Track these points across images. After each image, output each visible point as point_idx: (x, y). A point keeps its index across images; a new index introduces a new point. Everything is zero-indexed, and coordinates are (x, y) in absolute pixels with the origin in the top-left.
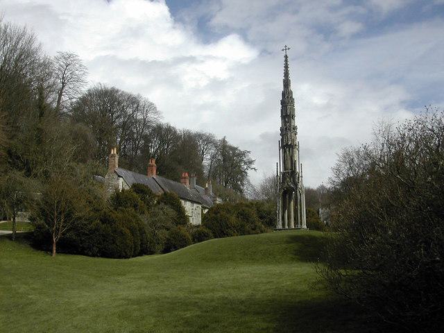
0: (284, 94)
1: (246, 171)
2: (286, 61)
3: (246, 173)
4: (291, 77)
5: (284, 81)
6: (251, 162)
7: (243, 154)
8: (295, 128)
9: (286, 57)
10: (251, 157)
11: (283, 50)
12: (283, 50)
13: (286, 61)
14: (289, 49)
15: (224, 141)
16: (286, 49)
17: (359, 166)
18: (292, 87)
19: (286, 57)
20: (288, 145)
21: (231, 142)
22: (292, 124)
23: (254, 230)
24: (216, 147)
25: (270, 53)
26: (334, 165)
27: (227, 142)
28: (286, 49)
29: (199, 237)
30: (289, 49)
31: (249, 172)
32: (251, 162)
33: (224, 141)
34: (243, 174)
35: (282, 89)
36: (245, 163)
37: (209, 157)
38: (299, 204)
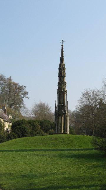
0: (60, 65)
2: (62, 48)
3: (23, 100)
4: (64, 57)
6: (26, 93)
8: (65, 83)
9: (62, 46)
10: (27, 89)
13: (62, 48)
14: (64, 42)
15: (10, 79)
16: (62, 42)
17: (93, 100)
18: (65, 62)
19: (62, 46)
20: (61, 92)
21: (15, 80)
23: (39, 134)
24: (5, 83)
26: (80, 99)
27: (12, 80)
28: (62, 42)
29: (9, 138)
30: (64, 42)
31: (25, 100)
32: (26, 93)
33: (10, 79)
34: (20, 101)
36: (23, 94)
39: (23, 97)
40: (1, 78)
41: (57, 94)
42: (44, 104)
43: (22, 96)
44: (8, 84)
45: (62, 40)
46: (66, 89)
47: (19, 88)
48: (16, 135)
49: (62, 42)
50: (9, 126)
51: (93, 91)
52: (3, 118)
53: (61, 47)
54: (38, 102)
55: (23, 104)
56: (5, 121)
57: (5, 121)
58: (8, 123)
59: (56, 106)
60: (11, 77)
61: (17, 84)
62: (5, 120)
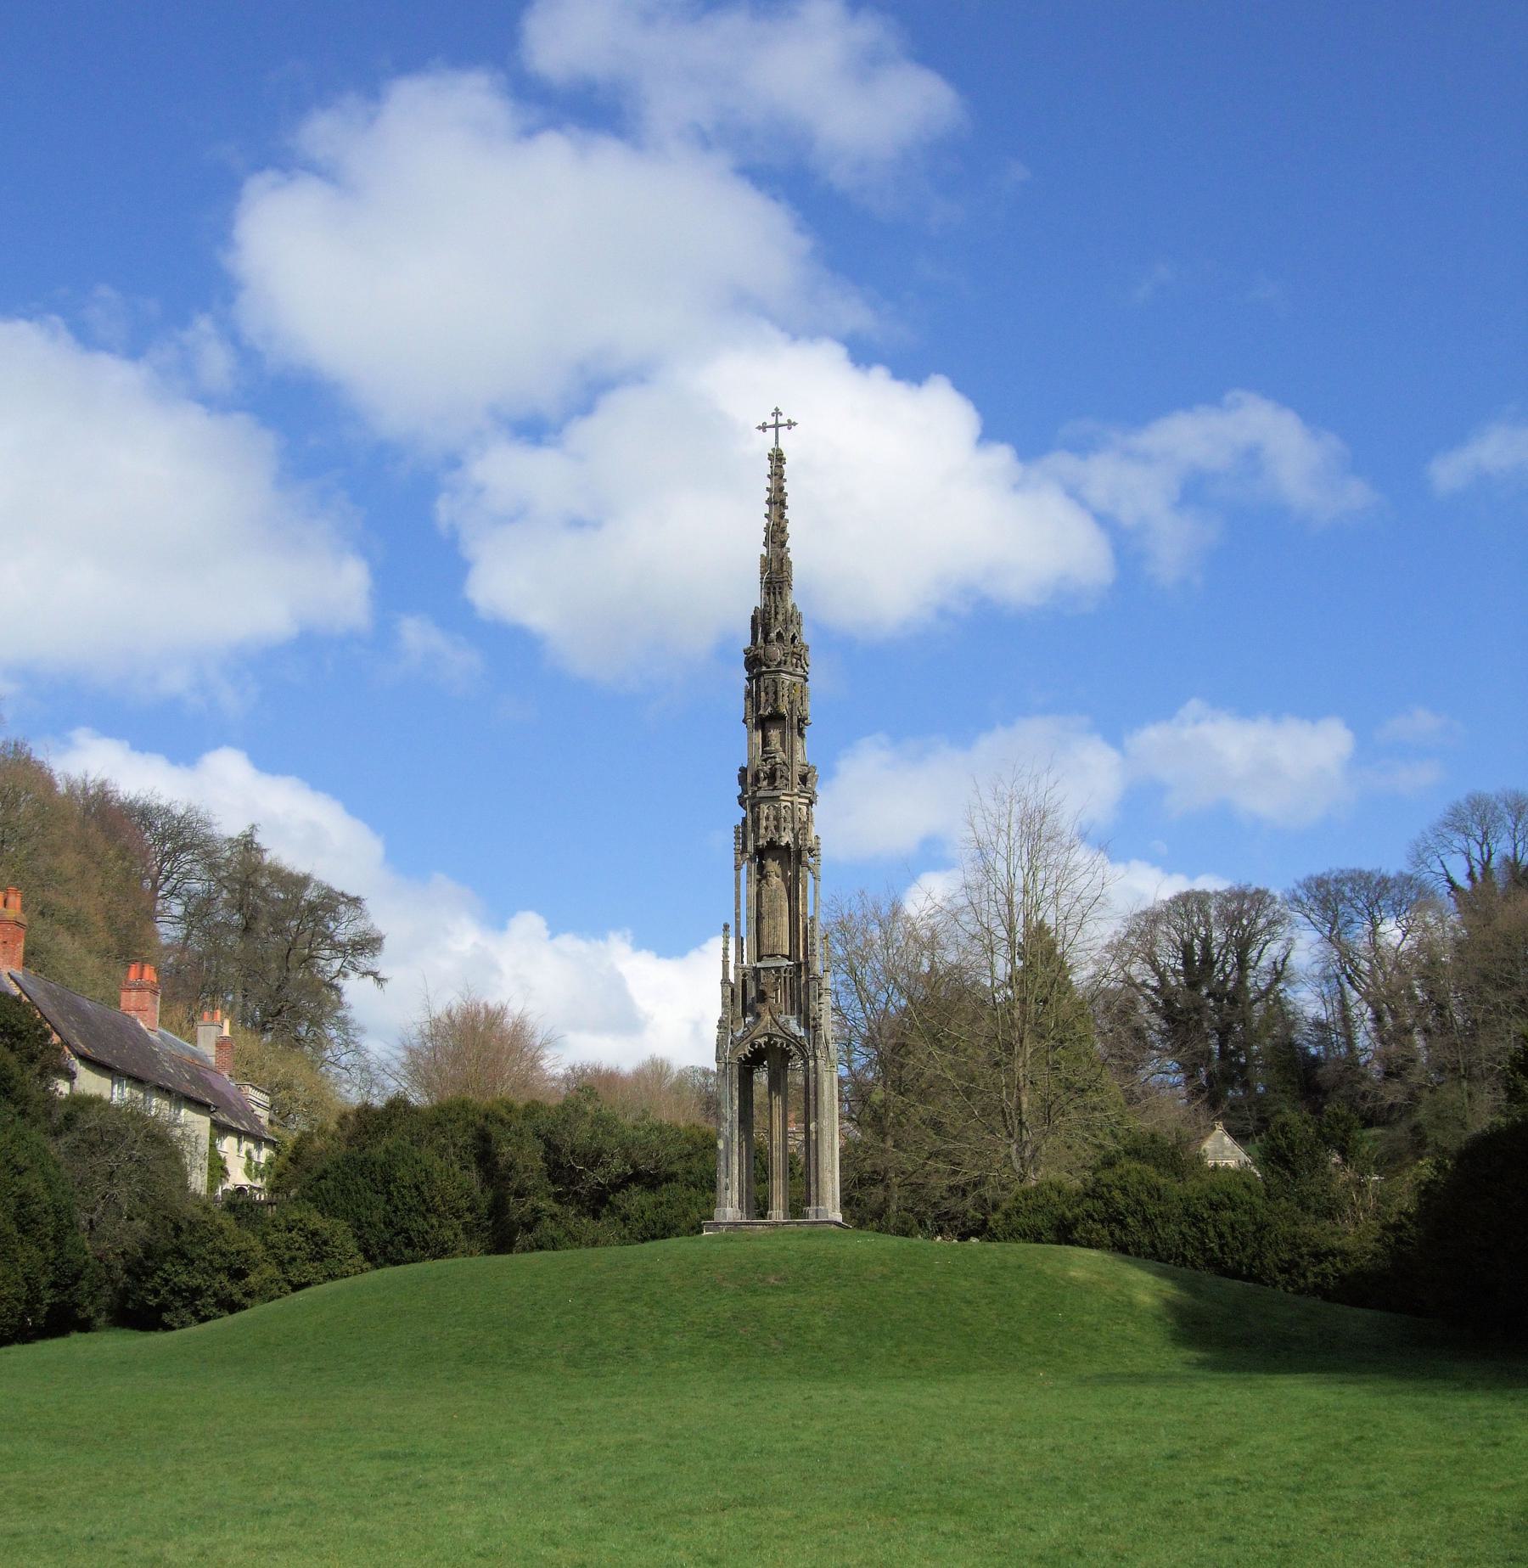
1: (340, 981)
2: (777, 475)
5: (766, 563)
6: (368, 944)
7: (332, 902)
9: (777, 458)
11: (764, 428)
12: (764, 428)
13: (777, 475)
14: (790, 424)
15: (247, 845)
16: (777, 426)
22: (799, 757)
24: (213, 867)
25: (512, 520)
27: (260, 851)
30: (790, 424)
31: (355, 989)
32: (368, 944)
33: (247, 845)
34: (325, 995)
35: (754, 598)
36: (340, 948)
37: (177, 909)
38: (813, 1188)
39: (342, 973)
40: (187, 834)
41: (737, 868)
42: (494, 1018)
43: (337, 964)
44: (230, 877)
45: (777, 413)
46: (814, 831)
47: (312, 908)
48: (340, 1232)
49: (777, 426)
50: (251, 1169)
51: (886, 910)
52: (199, 1106)
53: (766, 467)
54: (448, 1000)
55: (343, 1023)
56: (220, 1129)
57: (220, 1129)
58: (247, 1145)
59: (725, 981)
60: (253, 827)
61: (303, 882)
62: (224, 1118)
